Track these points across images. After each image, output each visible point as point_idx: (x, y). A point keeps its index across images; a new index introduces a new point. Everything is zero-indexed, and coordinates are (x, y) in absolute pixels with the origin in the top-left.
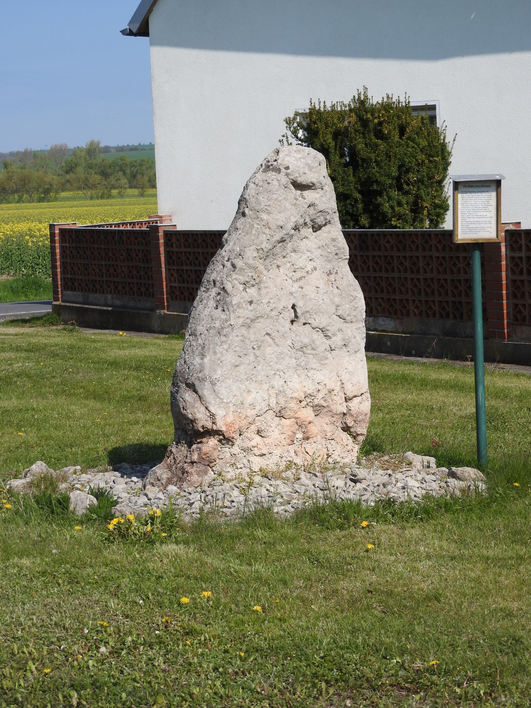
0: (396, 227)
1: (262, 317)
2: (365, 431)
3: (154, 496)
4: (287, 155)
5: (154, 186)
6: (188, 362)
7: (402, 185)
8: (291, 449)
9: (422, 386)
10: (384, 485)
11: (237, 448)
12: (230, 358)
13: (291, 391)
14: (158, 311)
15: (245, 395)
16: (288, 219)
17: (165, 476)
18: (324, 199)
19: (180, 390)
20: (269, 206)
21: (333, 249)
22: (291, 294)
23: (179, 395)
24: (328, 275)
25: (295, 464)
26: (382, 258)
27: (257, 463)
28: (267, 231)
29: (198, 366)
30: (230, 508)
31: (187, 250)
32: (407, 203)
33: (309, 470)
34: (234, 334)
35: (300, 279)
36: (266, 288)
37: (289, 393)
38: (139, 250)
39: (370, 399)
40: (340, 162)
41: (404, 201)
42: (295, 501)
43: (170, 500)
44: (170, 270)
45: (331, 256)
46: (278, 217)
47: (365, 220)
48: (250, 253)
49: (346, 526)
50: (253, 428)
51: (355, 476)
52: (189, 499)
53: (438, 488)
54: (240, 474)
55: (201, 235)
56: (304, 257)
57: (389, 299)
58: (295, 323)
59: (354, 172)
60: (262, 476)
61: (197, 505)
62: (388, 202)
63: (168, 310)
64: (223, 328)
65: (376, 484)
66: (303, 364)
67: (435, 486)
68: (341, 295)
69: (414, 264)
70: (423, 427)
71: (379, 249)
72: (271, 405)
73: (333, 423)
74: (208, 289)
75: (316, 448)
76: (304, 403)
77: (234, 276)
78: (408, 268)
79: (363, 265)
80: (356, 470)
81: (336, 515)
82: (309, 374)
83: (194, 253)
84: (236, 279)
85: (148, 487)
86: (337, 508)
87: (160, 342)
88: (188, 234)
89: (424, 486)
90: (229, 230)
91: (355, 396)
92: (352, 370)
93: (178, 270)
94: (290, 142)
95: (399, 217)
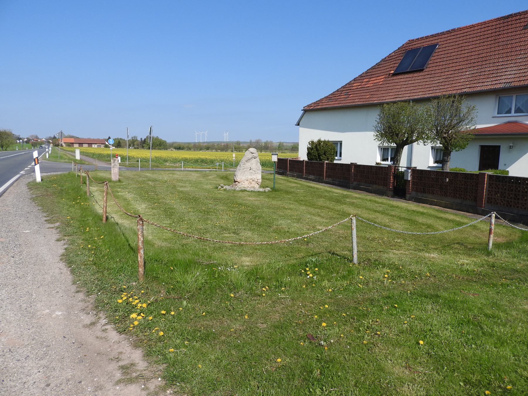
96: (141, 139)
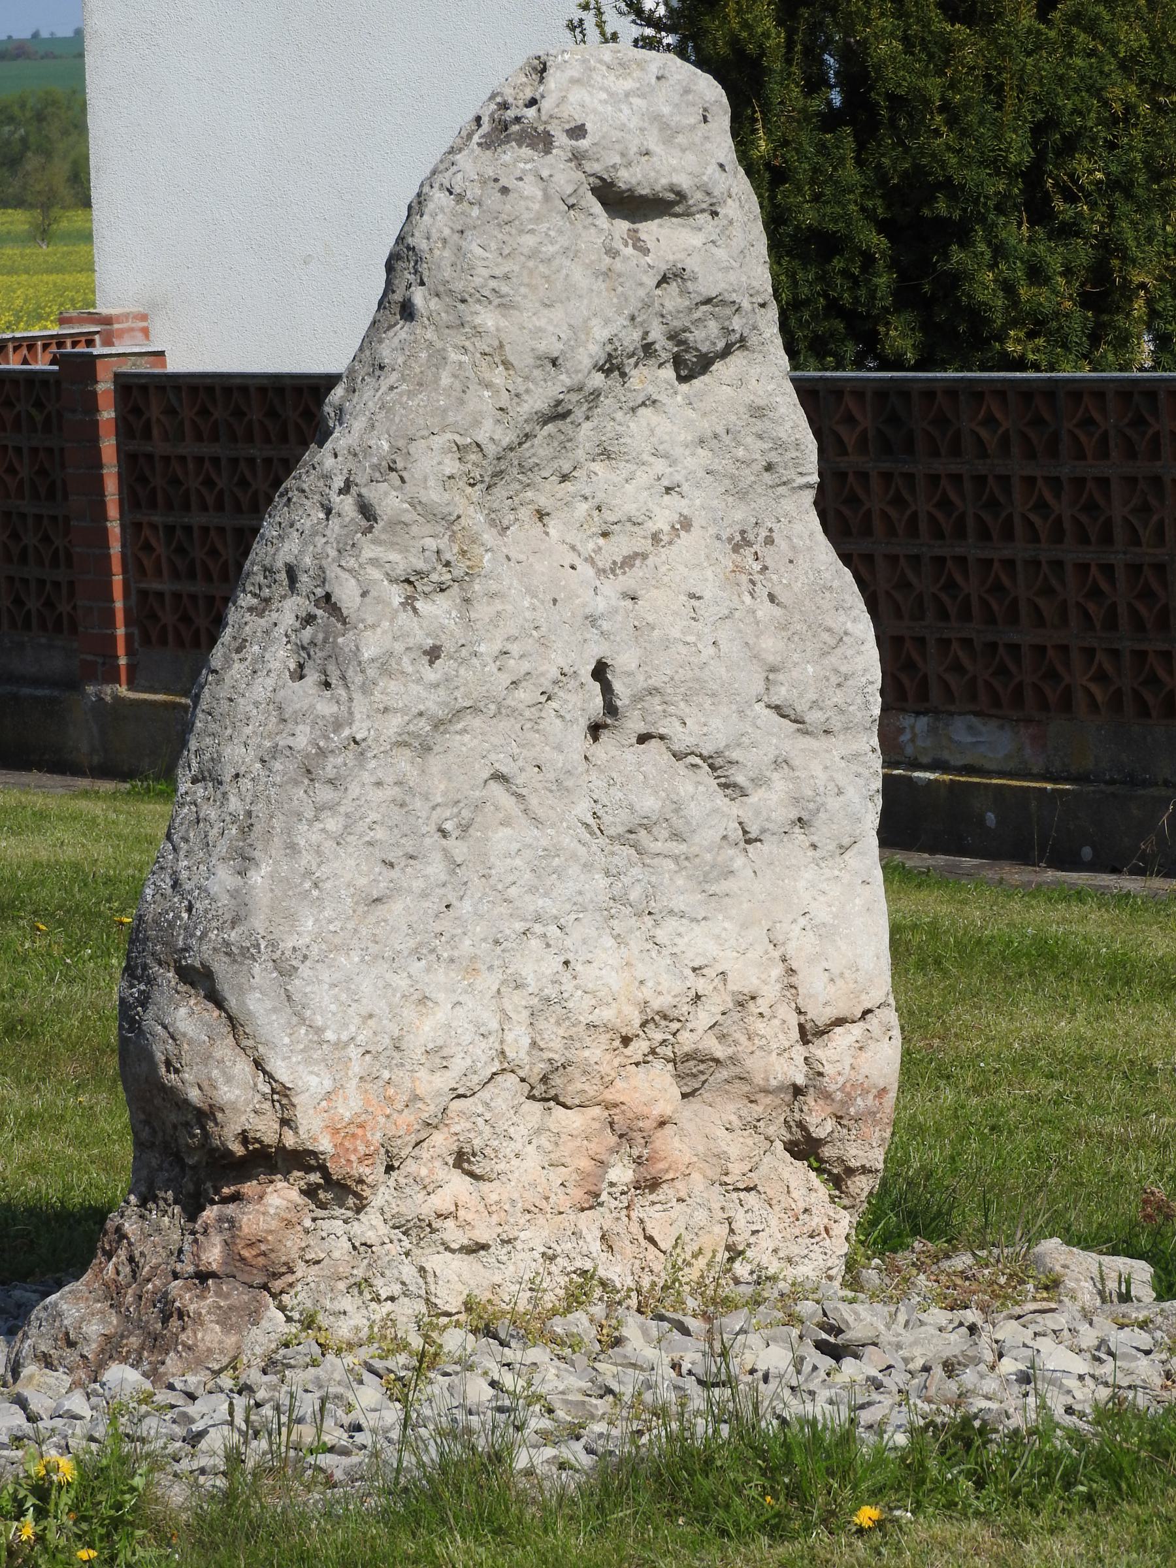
0: (1020, 364)
1: (475, 709)
2: (876, 1158)
3: (51, 1404)
4: (574, 81)
5: (87, 204)
6: (188, 886)
7: (1047, 198)
8: (590, 1224)
9: (1112, 982)
10: (950, 1368)
11: (377, 1220)
12: (349, 870)
13: (589, 1000)
14: (90, 689)
15: (409, 1013)
16: (579, 331)
17: (94, 1329)
18: (721, 253)
19: (156, 995)
20: (507, 277)
21: (755, 449)
22: (592, 620)
23: (152, 1010)
24: (736, 549)
25: (603, 1284)
26: (968, 485)
27: (455, 1279)
28: (498, 377)
29: (225, 900)
30: (345, 1452)
31: (207, 449)
32: (1068, 272)
33: (656, 1306)
34: (367, 777)
35: (628, 562)
36: (493, 596)
37: (580, 1005)
38: (18, 450)
39: (896, 1033)
40: (804, 110)
41: (1055, 264)
42: (599, 1427)
43: (113, 1420)
44: (138, 526)
45: (748, 476)
46: (542, 323)
47: (903, 336)
48: (432, 462)
49: (796, 1525)
50: (441, 1141)
51: (839, 1331)
52: (188, 1419)
53: (1158, 1381)
54: (390, 1320)
55: (262, 390)
56: (643, 478)
57: (993, 646)
58: (605, 735)
59: (861, 147)
60: (475, 1331)
61: (216, 1440)
62: (993, 266)
63: (132, 686)
64: (322, 753)
65: (918, 1363)
66: (635, 894)
67: (1147, 1370)
68: (785, 628)
69: (993, 504)
70: (1109, 1143)
71: (956, 450)
72: (511, 1054)
73: (753, 1126)
74: (267, 600)
75: (689, 1222)
76: (639, 1047)
77: (369, 551)
78: (1067, 525)
79: (893, 513)
80: (843, 1306)
81: (758, 1480)
82: (661, 935)
83: (234, 461)
84: (374, 562)
85: (30, 1369)
86: (761, 1453)
87: (96, 808)
88: (210, 389)
89: (1106, 1369)
90: (351, 370)
91: (840, 1022)
92: (828, 919)
93: (170, 529)
94: (609, 30)
95: (1037, 324)
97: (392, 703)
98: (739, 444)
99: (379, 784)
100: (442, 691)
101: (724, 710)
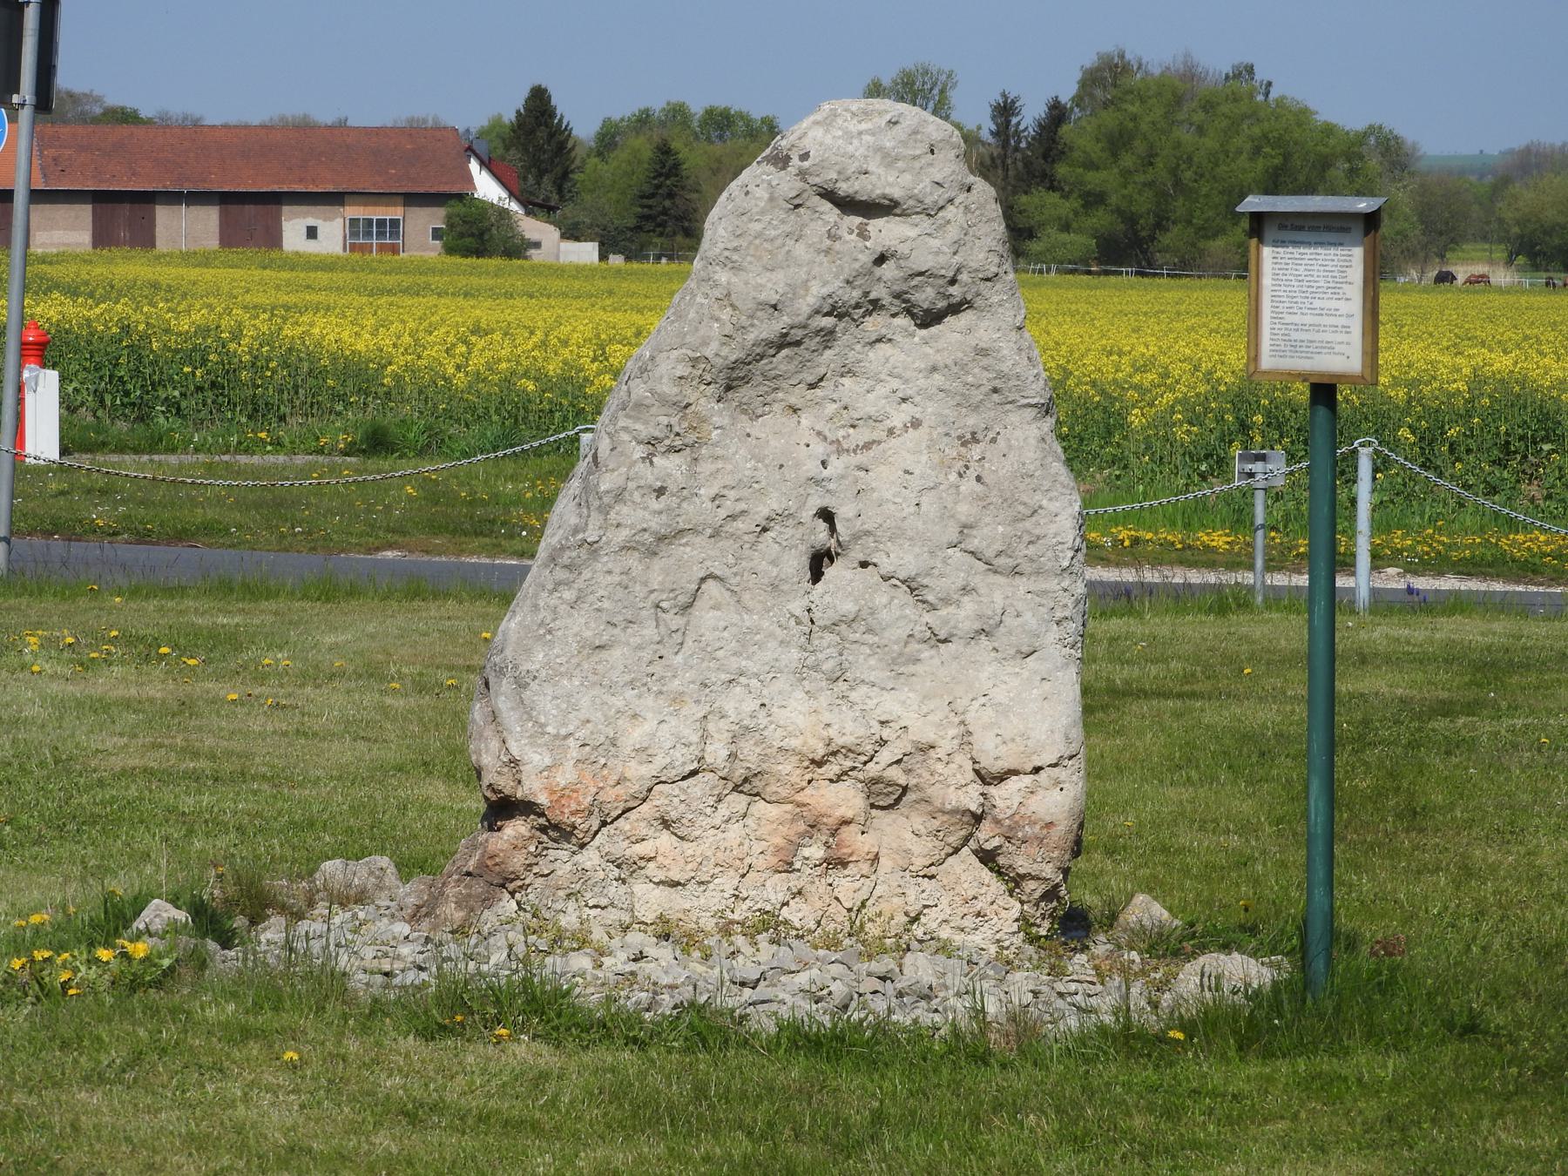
20: (735, 249)
27: (650, 900)
28: (725, 315)
35: (867, 446)
56: (881, 390)
82: (853, 696)
84: (625, 429)
96: (1005, 110)
97: (624, 522)
98: (968, 373)
99: (610, 572)
100: (664, 517)
101: (917, 550)
